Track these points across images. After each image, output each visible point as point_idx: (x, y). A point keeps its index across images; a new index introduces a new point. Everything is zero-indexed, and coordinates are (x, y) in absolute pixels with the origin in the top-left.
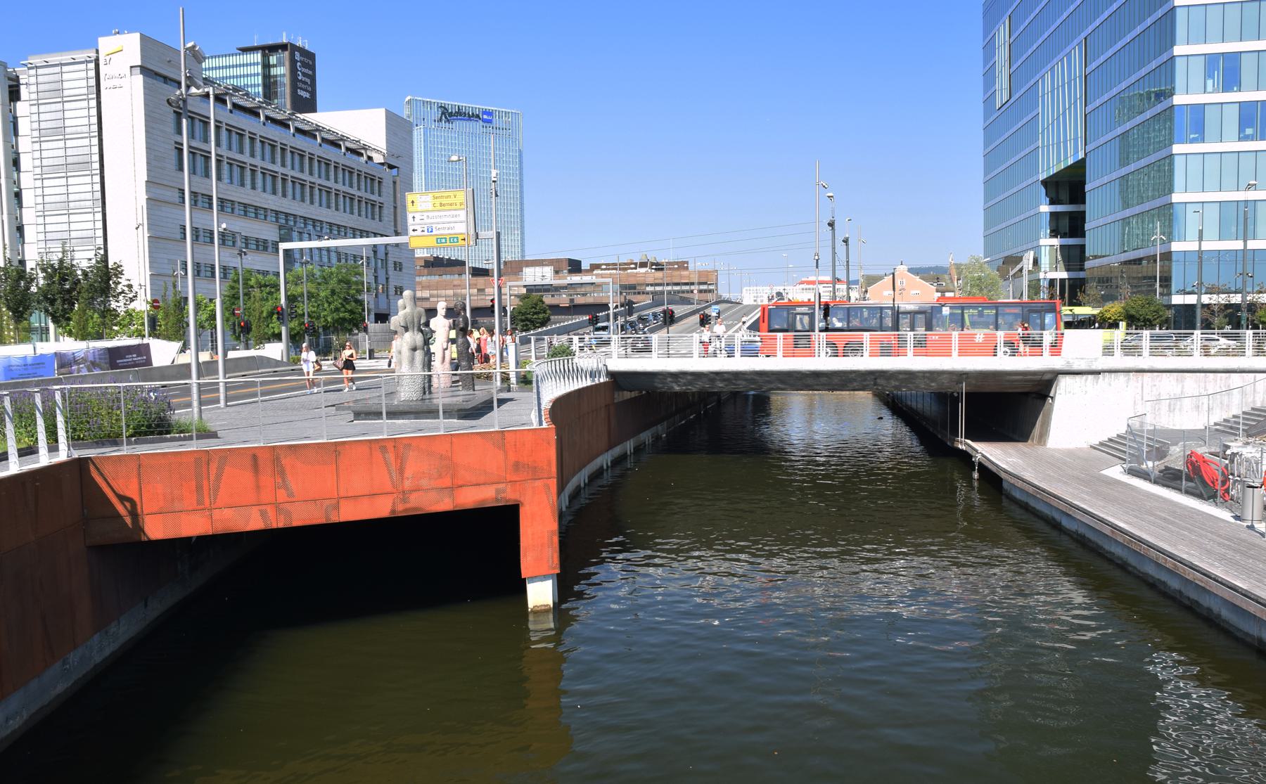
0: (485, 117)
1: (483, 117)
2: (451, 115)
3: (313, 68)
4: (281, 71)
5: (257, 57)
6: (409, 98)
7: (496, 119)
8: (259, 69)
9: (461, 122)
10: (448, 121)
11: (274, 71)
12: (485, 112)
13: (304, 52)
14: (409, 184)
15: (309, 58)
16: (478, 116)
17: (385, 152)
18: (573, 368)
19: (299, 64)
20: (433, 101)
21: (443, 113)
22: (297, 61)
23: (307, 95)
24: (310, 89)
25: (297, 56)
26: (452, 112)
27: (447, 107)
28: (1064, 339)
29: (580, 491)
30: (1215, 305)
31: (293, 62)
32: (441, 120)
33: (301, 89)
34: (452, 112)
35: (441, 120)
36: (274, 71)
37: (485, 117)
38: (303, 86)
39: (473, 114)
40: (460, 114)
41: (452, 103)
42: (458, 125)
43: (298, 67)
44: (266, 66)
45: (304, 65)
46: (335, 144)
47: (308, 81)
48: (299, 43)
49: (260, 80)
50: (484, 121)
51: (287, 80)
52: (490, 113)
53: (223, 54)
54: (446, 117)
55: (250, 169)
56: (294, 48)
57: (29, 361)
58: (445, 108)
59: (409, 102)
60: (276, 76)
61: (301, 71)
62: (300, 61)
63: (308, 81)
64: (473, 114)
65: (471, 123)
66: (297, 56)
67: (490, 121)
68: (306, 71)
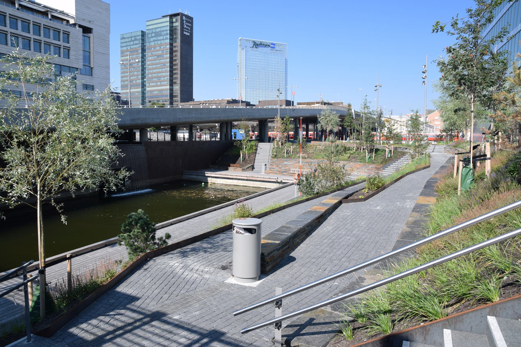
0: (272, 46)
1: (272, 46)
2: (257, 45)
3: (192, 23)
4: (177, 24)
5: (168, 19)
6: (240, 38)
7: (277, 48)
8: (168, 24)
9: (262, 48)
10: (256, 47)
11: (174, 25)
12: (272, 44)
13: (187, 16)
14: (108, 41)
15: (190, 20)
16: (269, 46)
17: (75, 17)
18: (146, 339)
19: (185, 21)
20: (250, 39)
21: (254, 44)
22: (184, 20)
23: (189, 34)
24: (190, 32)
25: (184, 18)
26: (258, 44)
27: (256, 42)
28: (119, 45)
29: (479, 300)
30: (280, 158)
31: (182, 20)
32: (253, 47)
33: (185, 31)
34: (258, 44)
35: (253, 47)
36: (174, 25)
37: (272, 46)
38: (187, 30)
39: (267, 45)
40: (261, 45)
41: (258, 40)
42: (260, 49)
43: (184, 23)
44: (171, 22)
45: (187, 21)
46: (45, 14)
47: (189, 28)
48: (186, 13)
49: (168, 28)
50: (272, 47)
51: (179, 28)
52: (274, 44)
53: (157, 18)
54: (255, 46)
55: (63, 48)
56: (182, 15)
57: (520, 130)
58: (255, 42)
59: (240, 40)
60: (176, 26)
61: (186, 24)
62: (185, 20)
63: (189, 28)
64: (267, 45)
65: (266, 48)
66: (184, 18)
67: (274, 48)
68: (188, 24)
